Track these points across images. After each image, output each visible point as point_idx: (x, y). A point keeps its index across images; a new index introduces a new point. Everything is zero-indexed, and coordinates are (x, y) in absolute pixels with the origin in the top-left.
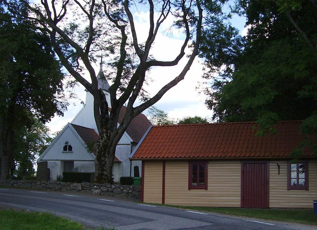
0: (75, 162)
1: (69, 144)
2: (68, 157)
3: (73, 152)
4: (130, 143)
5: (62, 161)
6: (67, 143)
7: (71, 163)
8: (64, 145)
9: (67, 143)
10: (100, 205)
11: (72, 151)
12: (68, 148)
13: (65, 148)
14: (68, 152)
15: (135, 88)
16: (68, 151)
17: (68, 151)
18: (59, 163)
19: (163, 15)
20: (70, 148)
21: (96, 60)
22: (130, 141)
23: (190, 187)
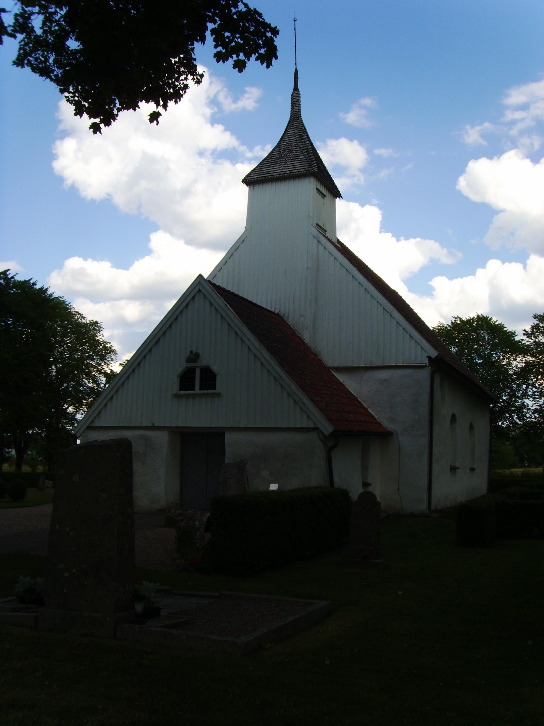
0: (229, 437)
1: (204, 361)
2: (198, 414)
3: (219, 395)
4: (426, 362)
5: (174, 431)
6: (194, 357)
7: (214, 437)
8: (180, 366)
9: (194, 357)
10: (324, 192)
11: (218, 390)
12: (197, 379)
13: (186, 381)
14: (200, 396)
15: (68, 68)
16: (197, 390)
17: (197, 390)
18: (162, 439)
19: (96, 424)
20: (209, 379)
21: (524, 334)
22: (425, 355)
23: (381, 232)
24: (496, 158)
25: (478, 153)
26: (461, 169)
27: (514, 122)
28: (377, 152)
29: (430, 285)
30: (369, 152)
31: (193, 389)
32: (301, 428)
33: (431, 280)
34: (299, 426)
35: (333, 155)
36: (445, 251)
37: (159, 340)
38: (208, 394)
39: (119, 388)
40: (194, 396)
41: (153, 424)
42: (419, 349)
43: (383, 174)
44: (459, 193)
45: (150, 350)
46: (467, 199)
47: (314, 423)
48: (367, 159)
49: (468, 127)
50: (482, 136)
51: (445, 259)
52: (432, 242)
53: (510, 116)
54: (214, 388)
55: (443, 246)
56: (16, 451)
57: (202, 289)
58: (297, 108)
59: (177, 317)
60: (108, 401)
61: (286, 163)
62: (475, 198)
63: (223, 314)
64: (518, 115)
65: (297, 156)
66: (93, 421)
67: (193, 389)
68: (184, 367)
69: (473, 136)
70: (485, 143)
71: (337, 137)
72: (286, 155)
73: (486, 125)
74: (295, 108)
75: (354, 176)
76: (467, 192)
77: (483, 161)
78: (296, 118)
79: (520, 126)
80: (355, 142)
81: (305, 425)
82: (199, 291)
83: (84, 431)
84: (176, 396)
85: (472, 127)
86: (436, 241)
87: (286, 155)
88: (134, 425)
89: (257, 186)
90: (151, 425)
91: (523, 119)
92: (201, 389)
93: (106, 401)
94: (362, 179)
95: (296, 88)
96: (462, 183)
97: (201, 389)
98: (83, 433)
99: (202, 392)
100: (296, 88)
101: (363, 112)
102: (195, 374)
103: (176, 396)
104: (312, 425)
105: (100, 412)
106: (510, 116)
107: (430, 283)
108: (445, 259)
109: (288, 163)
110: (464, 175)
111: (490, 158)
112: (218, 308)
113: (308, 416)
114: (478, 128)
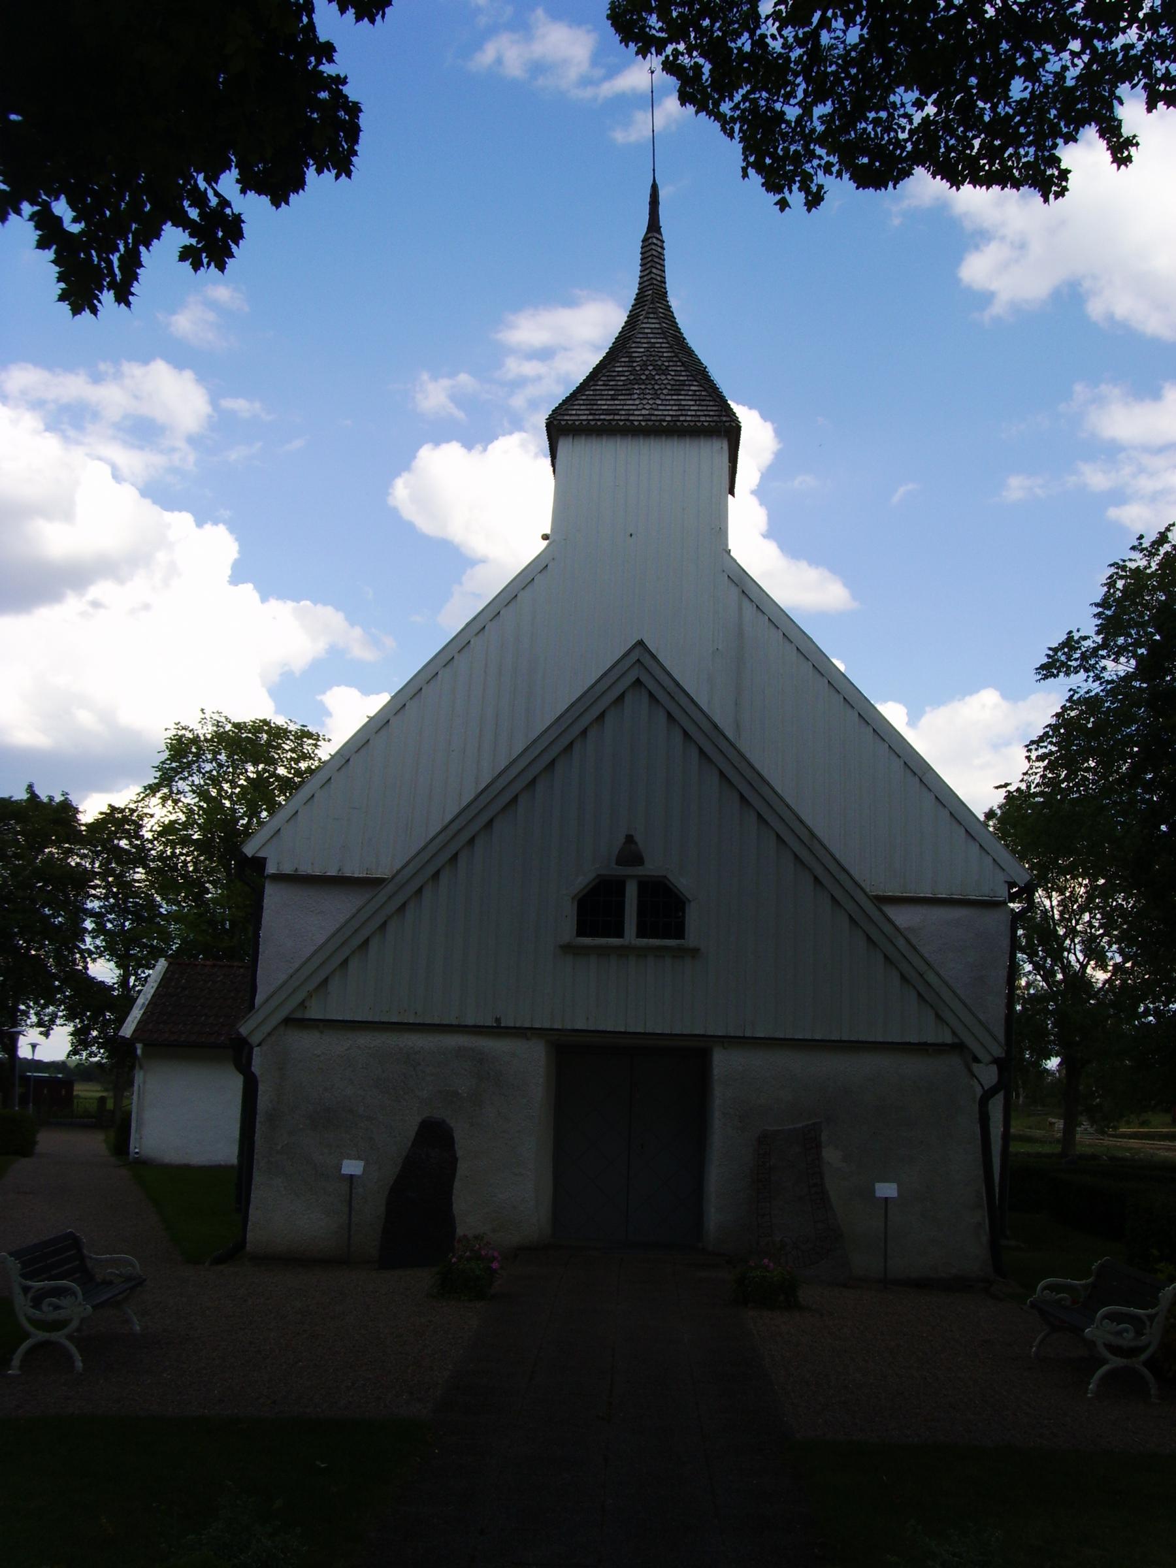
0: (723, 1062)
3: (694, 953)
9: (630, 854)
11: (692, 937)
13: (597, 910)
18: (530, 1063)
19: (315, 1012)
20: (664, 910)
22: (1001, 877)
24: (479, 447)
25: (440, 432)
26: (404, 461)
27: (520, 382)
28: (228, 404)
29: (321, 703)
30: (214, 402)
31: (620, 934)
32: (919, 1044)
33: (324, 693)
34: (913, 1039)
35: (136, 397)
36: (357, 632)
37: (515, 800)
38: (666, 948)
39: (390, 917)
40: (623, 952)
41: (498, 1020)
42: (988, 861)
43: (235, 455)
44: (394, 513)
45: (490, 824)
46: (410, 527)
47: (954, 1033)
48: (210, 417)
49: (425, 376)
50: (453, 398)
51: (361, 652)
52: (329, 610)
53: (515, 367)
54: (679, 933)
55: (352, 621)
56: (1065, 1123)
57: (645, 678)
58: (658, 272)
59: (571, 745)
60: (353, 952)
61: (656, 396)
62: (425, 525)
63: (708, 748)
64: (530, 368)
65: (683, 383)
66: (302, 1005)
67: (620, 934)
68: (591, 876)
69: (434, 396)
70: (460, 415)
71: (145, 359)
72: (650, 377)
73: (463, 378)
74: (654, 271)
75: (173, 450)
76: (409, 512)
77: (453, 451)
78: (651, 298)
79: (531, 391)
80: (188, 375)
81: (931, 1039)
82: (638, 682)
83: (275, 1028)
84: (568, 949)
85: (435, 378)
86: (337, 608)
87: (650, 377)
88: (437, 1021)
89: (688, 440)
90: (490, 1022)
91: (539, 378)
92: (641, 933)
93: (346, 952)
94: (192, 458)
95: (654, 226)
96: (401, 491)
97: (641, 933)
98: (269, 1034)
99: (644, 941)
100: (654, 226)
101: (211, 316)
102: (623, 895)
103: (568, 949)
104: (949, 1039)
105: (326, 981)
106: (515, 367)
107: (319, 698)
108: (361, 652)
109: (662, 397)
110: (406, 476)
111: (469, 446)
112: (692, 730)
113: (937, 1016)
114: (445, 382)
